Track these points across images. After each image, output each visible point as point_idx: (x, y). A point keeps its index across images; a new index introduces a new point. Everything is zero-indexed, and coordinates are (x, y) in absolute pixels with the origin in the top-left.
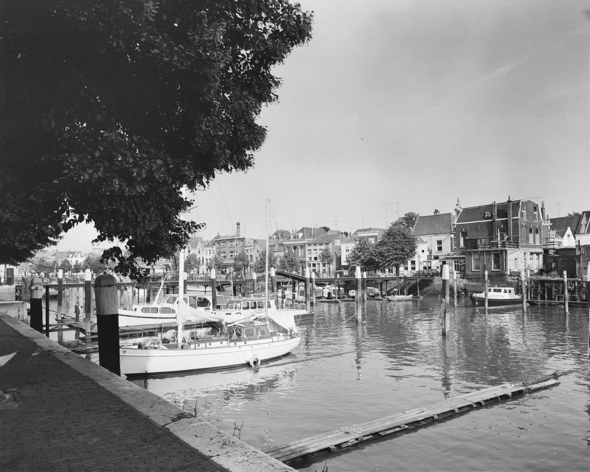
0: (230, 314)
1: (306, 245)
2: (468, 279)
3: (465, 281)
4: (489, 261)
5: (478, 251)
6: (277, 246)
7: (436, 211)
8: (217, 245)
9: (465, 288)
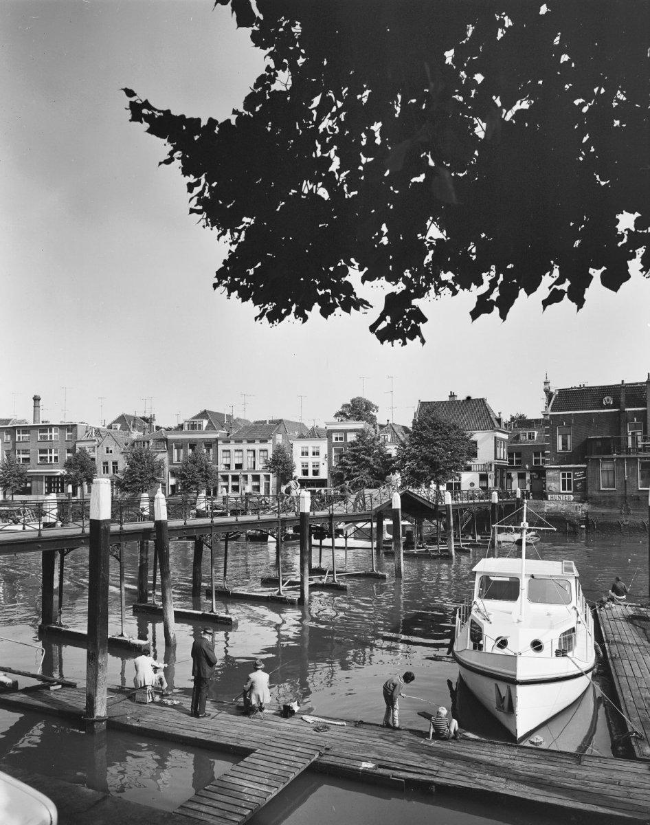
0: (347, 678)
2: (592, 503)
3: (585, 507)
4: (634, 474)
5: (613, 459)
6: (151, 442)
7: (452, 395)
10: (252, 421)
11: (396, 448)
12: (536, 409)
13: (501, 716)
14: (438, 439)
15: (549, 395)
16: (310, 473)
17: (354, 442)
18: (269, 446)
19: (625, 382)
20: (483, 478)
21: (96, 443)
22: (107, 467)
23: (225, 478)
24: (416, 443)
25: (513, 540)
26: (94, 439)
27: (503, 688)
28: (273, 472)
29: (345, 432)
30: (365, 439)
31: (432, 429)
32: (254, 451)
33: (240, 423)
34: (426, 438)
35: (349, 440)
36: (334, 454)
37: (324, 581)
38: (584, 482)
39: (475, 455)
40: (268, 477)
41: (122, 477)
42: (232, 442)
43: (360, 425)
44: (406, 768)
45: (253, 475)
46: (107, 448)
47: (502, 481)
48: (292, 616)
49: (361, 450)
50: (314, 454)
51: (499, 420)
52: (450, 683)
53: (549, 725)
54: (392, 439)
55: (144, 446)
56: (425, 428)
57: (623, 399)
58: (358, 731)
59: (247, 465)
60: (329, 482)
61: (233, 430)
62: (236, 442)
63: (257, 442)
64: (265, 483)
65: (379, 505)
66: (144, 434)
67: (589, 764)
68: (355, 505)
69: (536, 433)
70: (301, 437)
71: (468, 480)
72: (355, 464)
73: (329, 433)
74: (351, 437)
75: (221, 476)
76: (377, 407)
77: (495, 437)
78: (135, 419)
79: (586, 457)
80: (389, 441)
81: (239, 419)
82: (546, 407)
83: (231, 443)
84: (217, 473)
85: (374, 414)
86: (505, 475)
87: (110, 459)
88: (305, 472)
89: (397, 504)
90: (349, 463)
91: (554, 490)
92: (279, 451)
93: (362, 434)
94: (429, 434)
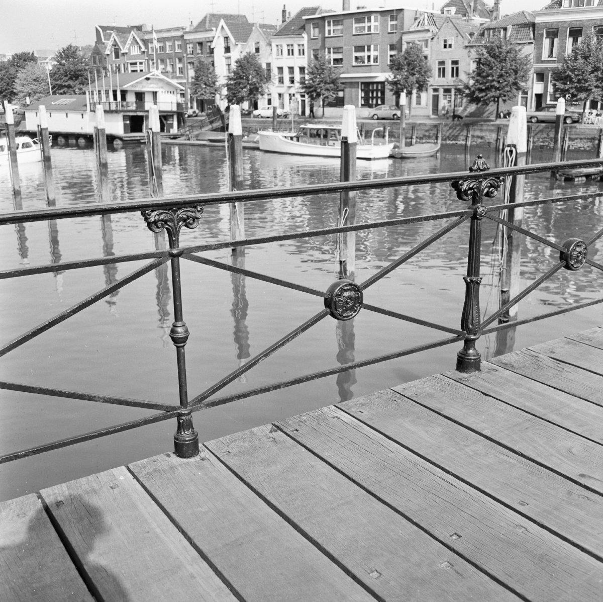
8: (315, 32)
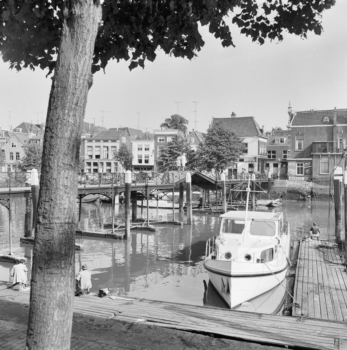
1: (86, 141)
2: (315, 182)
3: (311, 184)
7: (233, 114)
9: (312, 191)
10: (108, 128)
11: (196, 147)
12: (284, 124)
13: (224, 295)
14: (222, 142)
15: (292, 116)
16: (143, 161)
17: (171, 142)
18: (118, 145)
19: (337, 108)
20: (251, 166)
21: (5, 140)
22: (12, 156)
23: (89, 164)
24: (209, 144)
25: (266, 204)
26: (4, 137)
27: (225, 278)
28: (119, 161)
29: (166, 136)
30: (177, 140)
31: (219, 135)
32: (108, 147)
33: (99, 129)
34: (215, 140)
35: (168, 141)
36: (158, 150)
37: (143, 226)
38: (311, 169)
39: (246, 151)
40: (116, 164)
41: (22, 162)
42: (94, 141)
43: (175, 132)
44: (163, 321)
45: (106, 163)
46: (13, 144)
47: (262, 168)
48: (119, 246)
49: (174, 148)
50: (146, 150)
51: (261, 131)
52: (204, 281)
53: (253, 301)
54: (195, 141)
55: (36, 143)
56: (214, 134)
57: (335, 119)
58: (141, 303)
59: (103, 156)
60: (155, 167)
61: (95, 134)
62: (96, 141)
63: (110, 141)
64: (115, 168)
65: (178, 180)
66: (37, 135)
67: (265, 318)
68: (162, 179)
69: (285, 139)
70: (138, 139)
71: (242, 167)
72: (170, 156)
73: (156, 137)
74: (169, 140)
75: (87, 163)
76: (187, 121)
77: (259, 141)
78: (31, 125)
79: (312, 154)
80: (193, 142)
81: (99, 127)
82: (289, 123)
83: (101, 142)
84: (84, 161)
85: (186, 125)
86: (265, 165)
87: (14, 150)
88: (140, 161)
89: (189, 180)
90: (167, 155)
91: (292, 174)
92: (123, 148)
93: (175, 138)
94: (216, 138)
